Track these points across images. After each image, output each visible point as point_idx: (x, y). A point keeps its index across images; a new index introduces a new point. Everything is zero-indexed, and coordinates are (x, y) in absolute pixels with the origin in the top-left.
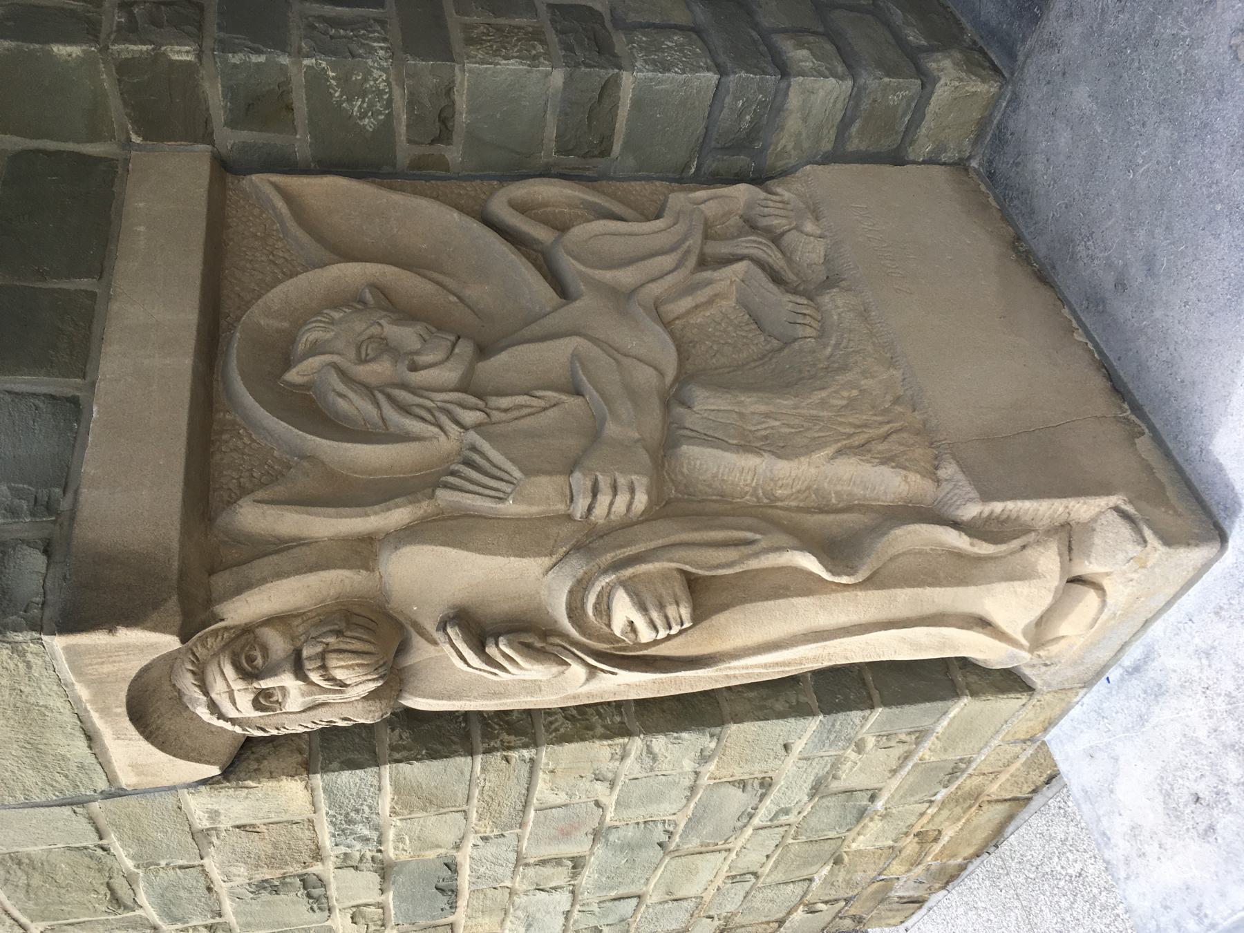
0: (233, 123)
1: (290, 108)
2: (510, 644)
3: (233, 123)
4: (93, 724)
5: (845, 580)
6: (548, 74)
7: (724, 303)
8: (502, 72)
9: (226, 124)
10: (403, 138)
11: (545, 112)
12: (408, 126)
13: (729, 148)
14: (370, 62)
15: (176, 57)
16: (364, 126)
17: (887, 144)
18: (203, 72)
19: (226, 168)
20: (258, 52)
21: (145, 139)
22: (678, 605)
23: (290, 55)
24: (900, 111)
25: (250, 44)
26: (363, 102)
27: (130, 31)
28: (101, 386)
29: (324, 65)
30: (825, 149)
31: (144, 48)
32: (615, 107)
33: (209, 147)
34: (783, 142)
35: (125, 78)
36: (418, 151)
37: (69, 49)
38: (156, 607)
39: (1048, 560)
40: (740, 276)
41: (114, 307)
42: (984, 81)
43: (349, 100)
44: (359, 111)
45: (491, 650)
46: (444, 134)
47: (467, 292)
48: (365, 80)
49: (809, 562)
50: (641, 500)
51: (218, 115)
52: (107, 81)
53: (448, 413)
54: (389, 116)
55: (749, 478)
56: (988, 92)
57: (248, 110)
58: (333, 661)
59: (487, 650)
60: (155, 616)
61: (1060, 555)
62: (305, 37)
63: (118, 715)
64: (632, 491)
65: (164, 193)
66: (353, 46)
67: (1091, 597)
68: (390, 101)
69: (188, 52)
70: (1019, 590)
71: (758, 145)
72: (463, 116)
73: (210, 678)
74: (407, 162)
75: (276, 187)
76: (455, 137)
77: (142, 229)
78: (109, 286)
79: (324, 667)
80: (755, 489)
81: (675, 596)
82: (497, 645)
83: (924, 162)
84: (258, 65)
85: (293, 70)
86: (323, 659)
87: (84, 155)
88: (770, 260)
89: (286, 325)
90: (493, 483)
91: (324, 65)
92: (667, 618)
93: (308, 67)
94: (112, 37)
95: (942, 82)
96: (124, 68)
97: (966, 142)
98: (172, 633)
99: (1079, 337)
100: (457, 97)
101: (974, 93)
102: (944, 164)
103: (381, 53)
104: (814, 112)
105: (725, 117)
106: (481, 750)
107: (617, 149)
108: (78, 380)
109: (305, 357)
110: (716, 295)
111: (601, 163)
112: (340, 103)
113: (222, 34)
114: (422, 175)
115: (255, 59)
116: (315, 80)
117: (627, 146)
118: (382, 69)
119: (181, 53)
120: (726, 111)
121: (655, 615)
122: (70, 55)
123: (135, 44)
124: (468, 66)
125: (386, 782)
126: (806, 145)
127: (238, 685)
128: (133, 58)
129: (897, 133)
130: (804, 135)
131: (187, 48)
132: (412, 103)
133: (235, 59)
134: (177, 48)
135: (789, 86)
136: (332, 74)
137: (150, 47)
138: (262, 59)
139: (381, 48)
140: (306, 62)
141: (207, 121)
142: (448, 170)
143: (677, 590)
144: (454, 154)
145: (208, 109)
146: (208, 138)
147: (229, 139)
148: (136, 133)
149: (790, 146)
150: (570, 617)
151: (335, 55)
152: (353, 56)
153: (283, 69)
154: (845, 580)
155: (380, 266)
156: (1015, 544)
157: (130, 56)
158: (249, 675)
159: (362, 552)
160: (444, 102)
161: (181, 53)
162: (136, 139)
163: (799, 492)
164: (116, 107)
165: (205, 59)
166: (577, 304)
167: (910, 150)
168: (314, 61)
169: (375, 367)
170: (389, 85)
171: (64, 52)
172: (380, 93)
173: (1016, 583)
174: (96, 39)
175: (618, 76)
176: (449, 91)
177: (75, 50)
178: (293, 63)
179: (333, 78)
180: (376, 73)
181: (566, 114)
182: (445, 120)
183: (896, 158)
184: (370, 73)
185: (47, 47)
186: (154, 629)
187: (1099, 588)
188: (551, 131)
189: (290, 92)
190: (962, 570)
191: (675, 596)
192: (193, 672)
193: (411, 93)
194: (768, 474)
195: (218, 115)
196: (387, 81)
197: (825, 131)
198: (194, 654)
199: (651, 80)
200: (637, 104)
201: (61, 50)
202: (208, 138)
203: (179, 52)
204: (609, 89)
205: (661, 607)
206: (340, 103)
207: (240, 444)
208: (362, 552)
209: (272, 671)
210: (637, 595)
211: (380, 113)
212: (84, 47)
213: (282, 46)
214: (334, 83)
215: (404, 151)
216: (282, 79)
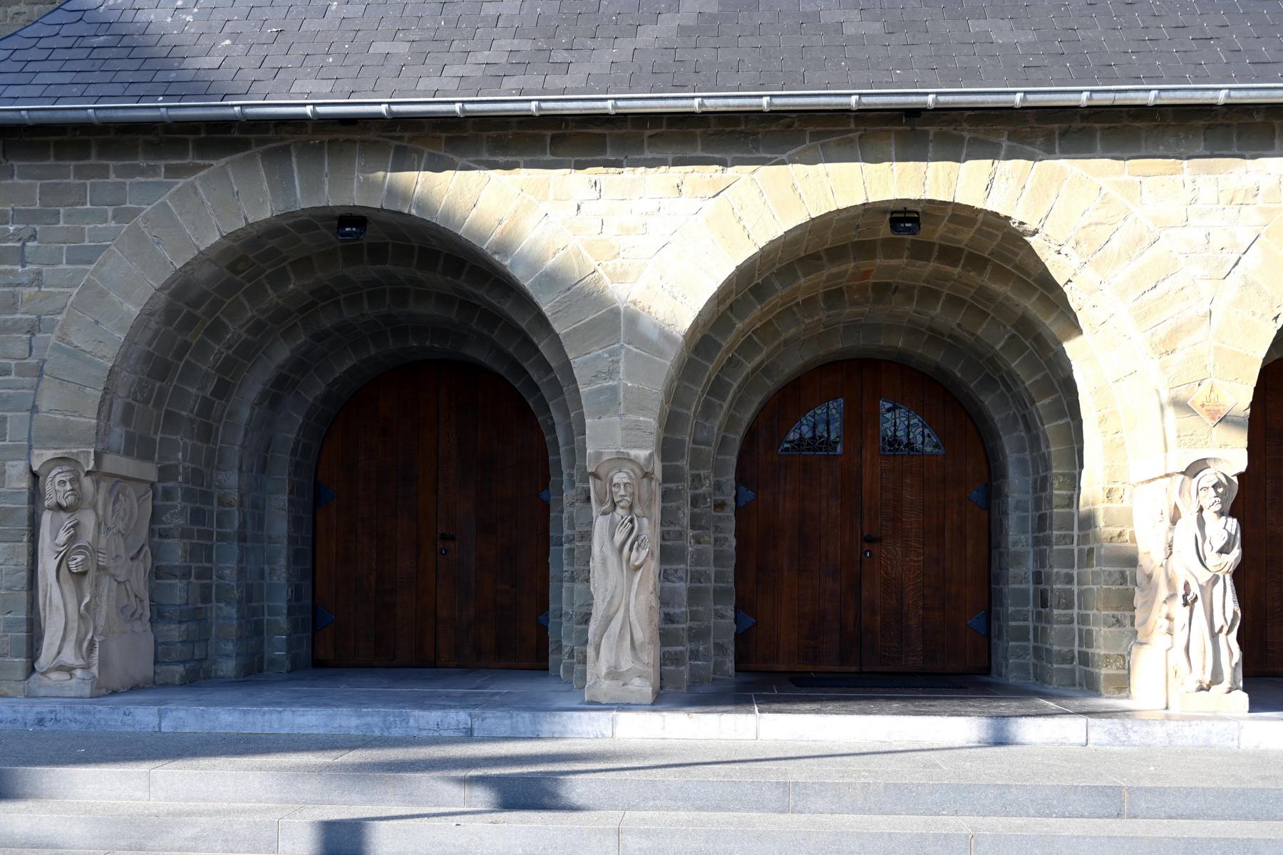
19: (152, 484)
27: (184, 468)
49: (86, 600)
51: (165, 485)
65: (149, 471)
72: (166, 541)
96: (177, 466)
114: (152, 532)
116: (175, 507)
119: (180, 479)
144: (156, 539)
147: (160, 486)
158: (70, 481)
159: (95, 507)
161: (180, 479)
182: (166, 537)
190: (79, 643)
195: (165, 485)
204: (175, 577)
208: (95, 507)
215: (156, 527)
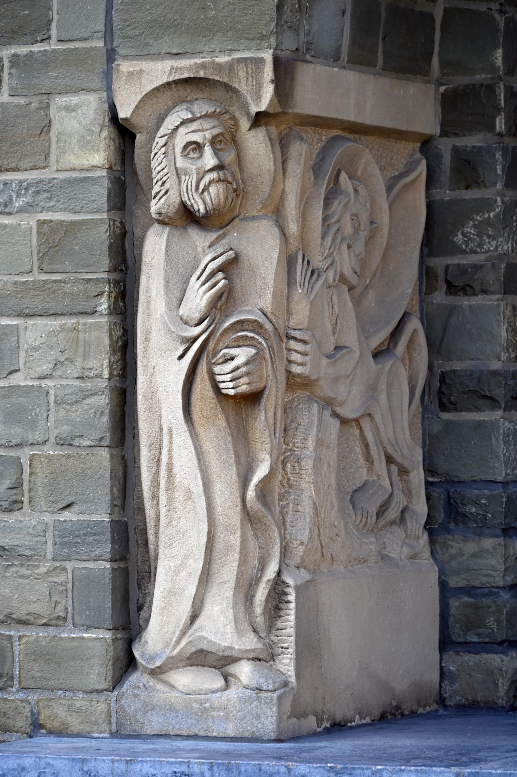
0: (455, 150)
1: (467, 187)
2: (224, 286)
3: (455, 150)
4: (189, 58)
5: (251, 493)
6: (499, 358)
7: (365, 471)
8: (499, 326)
9: (454, 146)
10: (449, 262)
11: (473, 360)
12: (459, 265)
13: (449, 503)
14: (500, 240)
15: (498, 120)
16: (457, 235)
17: (457, 632)
18: (490, 135)
19: (426, 144)
20: (503, 170)
21: (442, 94)
22: (248, 384)
23: (503, 189)
24: (480, 631)
25: (507, 165)
26: (474, 235)
27: (510, 92)
28: (344, 72)
29: (497, 210)
30: (450, 581)
31: (502, 102)
32: (478, 409)
33: (438, 134)
34: (455, 544)
35: (483, 88)
36: (441, 273)
37: (500, 59)
38: (279, 101)
39: (250, 642)
40: (382, 483)
41: (372, 77)
42: (507, 692)
43: (475, 226)
44: (468, 232)
45: (220, 275)
46: (452, 289)
47: (371, 292)
48: (489, 236)
49: (262, 471)
50: (296, 369)
52: (480, 78)
53: (332, 264)
54: (464, 252)
55: (299, 445)
56: (498, 698)
57: (466, 161)
58: (221, 187)
59: (220, 273)
60: (276, 101)
61: (254, 650)
62: (512, 200)
63: (197, 72)
64: (302, 364)
66: (508, 229)
67: (220, 683)
68: (475, 252)
69: (501, 128)
70: (229, 627)
71: (452, 526)
72: (465, 302)
73: (211, 120)
74: (431, 265)
75: (419, 176)
76: (452, 297)
77: (402, 92)
78: (380, 75)
79: (220, 180)
80: (291, 450)
81: (253, 382)
82: (224, 278)
83: (441, 668)
84: (495, 169)
85: (493, 191)
86: (223, 181)
87: (432, 56)
88: (390, 509)
89: (359, 174)
90: (307, 282)
91: (497, 210)
92: (241, 377)
93: (496, 200)
94: (507, 84)
95: (504, 658)
97: (458, 698)
98: (267, 108)
99: (357, 721)
100: (480, 297)
101: (497, 686)
102: (440, 686)
103: (506, 248)
104: (479, 561)
105: (471, 493)
106: (110, 278)
107: (446, 416)
108: (346, 60)
109: (353, 184)
110: (372, 463)
111: (435, 407)
112: (473, 220)
113: (511, 148)
115: (499, 168)
116: (487, 205)
117: (449, 423)
118: (497, 247)
119: (500, 124)
120: (478, 492)
121: (243, 369)
122: (496, 58)
123: (505, 97)
124: (502, 304)
125: (97, 216)
126: (453, 564)
127: (208, 135)
128: (496, 95)
129: (465, 635)
130: (461, 559)
131: (503, 128)
132: (477, 268)
133: (498, 156)
134: (503, 121)
135: (497, 536)
136: (492, 215)
137: (503, 105)
138: (499, 172)
139: (508, 248)
140: (499, 199)
141: (457, 135)
142: (426, 293)
143: (256, 384)
144: (440, 297)
145: (464, 136)
146: (444, 133)
147: (445, 147)
148: (446, 90)
149: (453, 551)
150: (237, 322)
151: (504, 217)
152: (503, 229)
153: (495, 184)
154: (251, 493)
155: (387, 235)
156: (260, 620)
157: (497, 93)
158: (214, 142)
159: (277, 214)
160: (477, 288)
161: (500, 124)
162: (442, 89)
163: (289, 479)
164: (462, 80)
165: (497, 137)
166: (372, 359)
167: (451, 653)
168: (500, 204)
169: (349, 223)
170: (486, 252)
171: (498, 55)
172: (481, 246)
173: (233, 624)
174: (506, 74)
175: (500, 407)
176: (484, 292)
177: (499, 62)
178: (498, 191)
179: (489, 216)
180: (494, 243)
181: (471, 375)
182: (467, 289)
183: (446, 643)
184: (494, 239)
185: (501, 46)
186: (271, 101)
187: (227, 686)
188: (458, 366)
189: (479, 187)
191: (253, 382)
192: (215, 111)
193: (481, 266)
194: (303, 456)
196: (489, 251)
197: (463, 576)
198: (225, 113)
199: (498, 433)
200: (480, 425)
201: (499, 53)
202: (444, 133)
203: (501, 123)
205: (247, 374)
206: (473, 220)
207: (315, 143)
208: (277, 214)
209: (216, 152)
210: (254, 360)
211: (467, 246)
212: (501, 68)
213: (507, 185)
214: (486, 216)
215: (439, 263)
216: (487, 184)
